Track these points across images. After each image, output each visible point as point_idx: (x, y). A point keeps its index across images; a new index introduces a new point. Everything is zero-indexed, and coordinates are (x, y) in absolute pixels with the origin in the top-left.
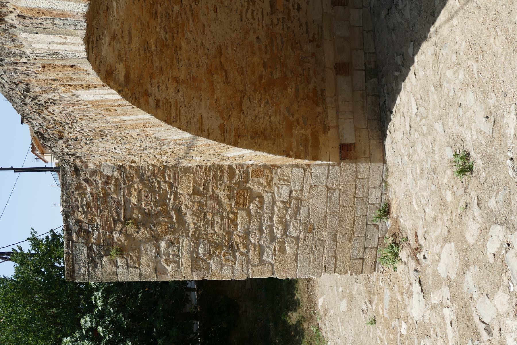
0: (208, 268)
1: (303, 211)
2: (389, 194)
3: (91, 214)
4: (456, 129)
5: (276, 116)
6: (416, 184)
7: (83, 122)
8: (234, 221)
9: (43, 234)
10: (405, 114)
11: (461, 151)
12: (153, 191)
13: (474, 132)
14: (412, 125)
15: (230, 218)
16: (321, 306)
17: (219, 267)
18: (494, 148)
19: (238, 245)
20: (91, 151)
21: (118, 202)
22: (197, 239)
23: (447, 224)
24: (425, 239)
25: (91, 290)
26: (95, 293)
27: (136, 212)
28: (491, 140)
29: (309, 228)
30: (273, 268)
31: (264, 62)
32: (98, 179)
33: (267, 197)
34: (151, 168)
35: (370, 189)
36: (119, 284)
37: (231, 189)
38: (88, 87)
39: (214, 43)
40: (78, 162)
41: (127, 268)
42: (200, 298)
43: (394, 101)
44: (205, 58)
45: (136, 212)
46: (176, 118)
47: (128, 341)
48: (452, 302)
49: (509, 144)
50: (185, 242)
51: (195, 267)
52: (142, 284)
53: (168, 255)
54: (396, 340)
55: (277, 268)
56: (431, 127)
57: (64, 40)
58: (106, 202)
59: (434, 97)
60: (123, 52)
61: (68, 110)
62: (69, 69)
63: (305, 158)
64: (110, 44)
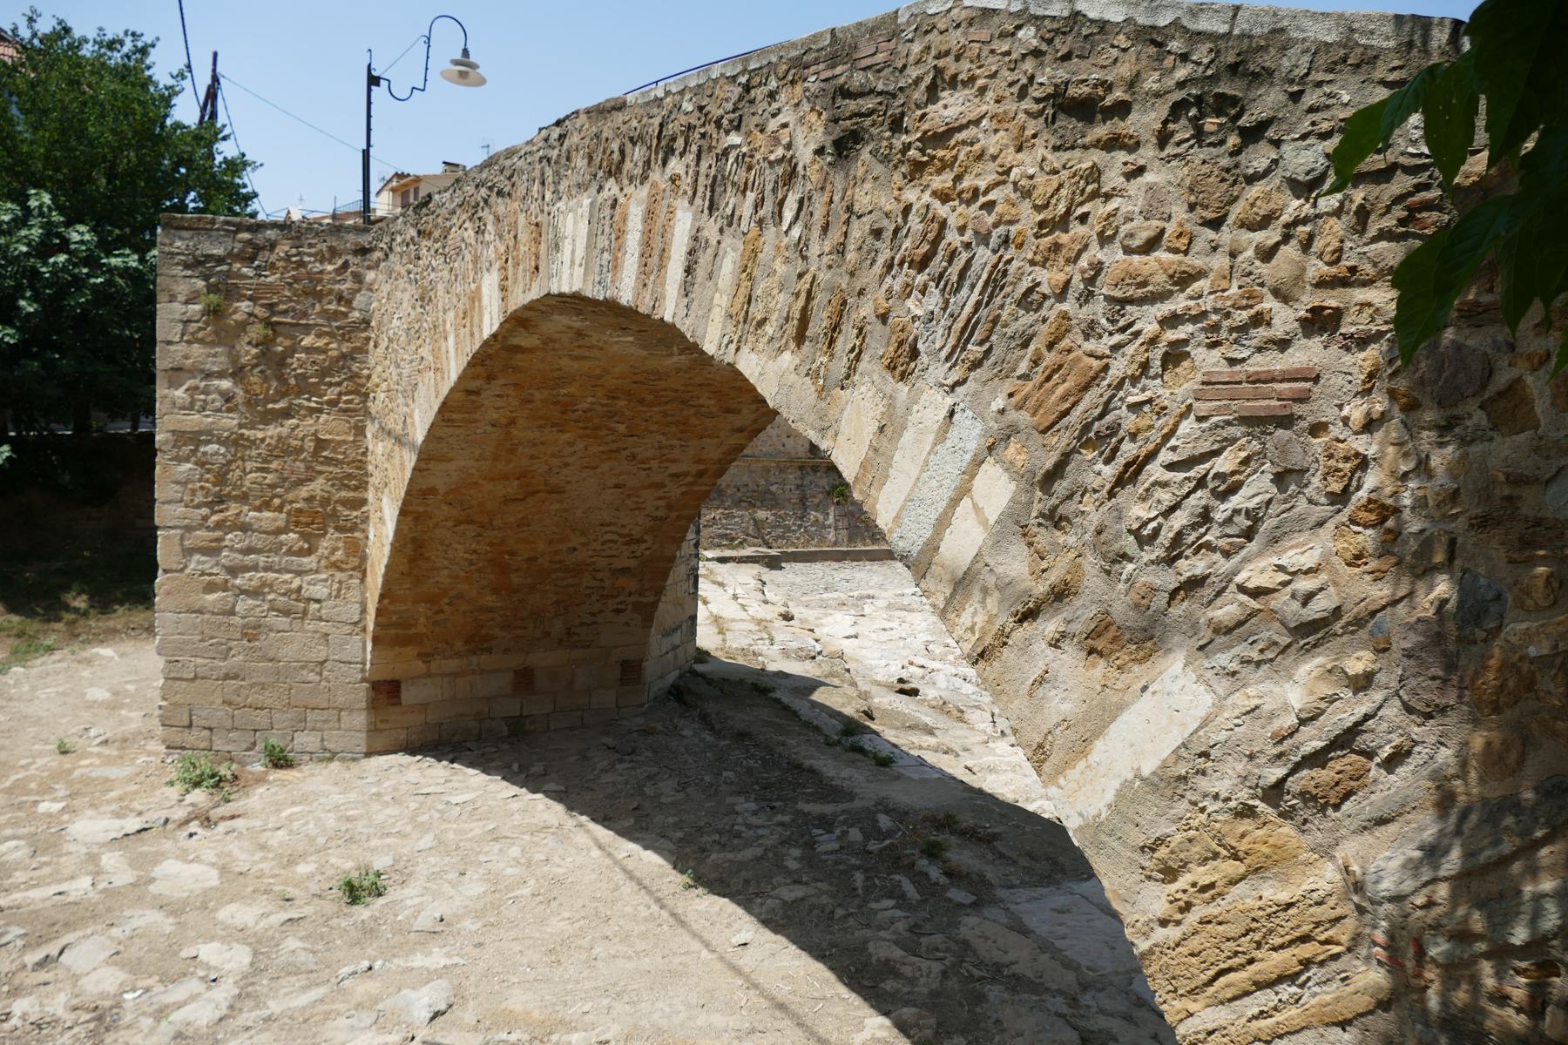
0: (180, 460)
1: (282, 622)
2: (311, 766)
3: (285, 268)
4: (422, 870)
5: (449, 577)
6: (329, 811)
7: (446, 273)
8: (266, 505)
9: (251, 180)
10: (449, 785)
11: (384, 883)
12: (323, 373)
13: (416, 901)
14: (430, 797)
15: (272, 498)
16: (97, 654)
17: (181, 478)
18: (390, 936)
19: (221, 511)
20: (396, 279)
21: (305, 315)
22: (236, 443)
23: (255, 869)
24: (227, 833)
25: (142, 249)
26: (136, 257)
27: (288, 343)
28: (400, 930)
29: (251, 632)
30: (176, 571)
31: (536, 559)
32: (348, 285)
33: (309, 562)
34: (365, 372)
35: (319, 733)
36: (151, 299)
37: (325, 502)
38: (503, 289)
39: (568, 482)
40: (378, 255)
41: (181, 321)
42: (120, 439)
43: (471, 765)
44: (546, 468)
45: (288, 343)
46: (448, 420)
47: (35, 306)
48: (104, 891)
49: (396, 961)
50: (230, 422)
51: (181, 437)
52: (150, 341)
53: (206, 392)
54: (27, 795)
55: (177, 578)
56: (425, 828)
57: (577, 262)
58: (306, 294)
59: (477, 829)
60: (557, 346)
61: (466, 252)
62: (533, 264)
63: (377, 624)
64: (570, 328)
